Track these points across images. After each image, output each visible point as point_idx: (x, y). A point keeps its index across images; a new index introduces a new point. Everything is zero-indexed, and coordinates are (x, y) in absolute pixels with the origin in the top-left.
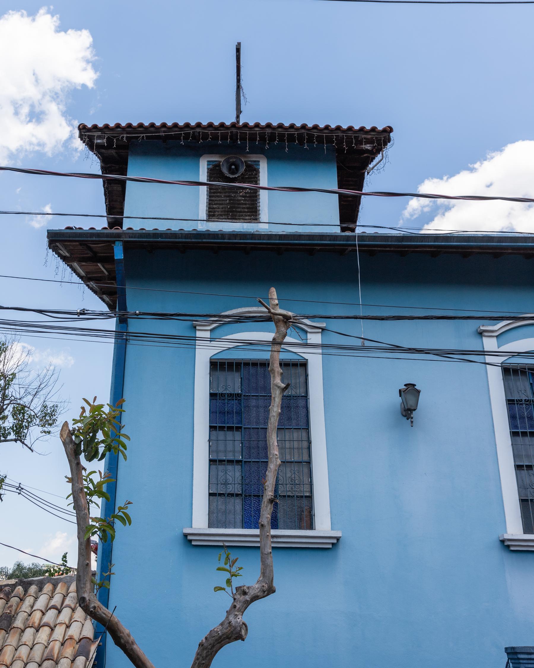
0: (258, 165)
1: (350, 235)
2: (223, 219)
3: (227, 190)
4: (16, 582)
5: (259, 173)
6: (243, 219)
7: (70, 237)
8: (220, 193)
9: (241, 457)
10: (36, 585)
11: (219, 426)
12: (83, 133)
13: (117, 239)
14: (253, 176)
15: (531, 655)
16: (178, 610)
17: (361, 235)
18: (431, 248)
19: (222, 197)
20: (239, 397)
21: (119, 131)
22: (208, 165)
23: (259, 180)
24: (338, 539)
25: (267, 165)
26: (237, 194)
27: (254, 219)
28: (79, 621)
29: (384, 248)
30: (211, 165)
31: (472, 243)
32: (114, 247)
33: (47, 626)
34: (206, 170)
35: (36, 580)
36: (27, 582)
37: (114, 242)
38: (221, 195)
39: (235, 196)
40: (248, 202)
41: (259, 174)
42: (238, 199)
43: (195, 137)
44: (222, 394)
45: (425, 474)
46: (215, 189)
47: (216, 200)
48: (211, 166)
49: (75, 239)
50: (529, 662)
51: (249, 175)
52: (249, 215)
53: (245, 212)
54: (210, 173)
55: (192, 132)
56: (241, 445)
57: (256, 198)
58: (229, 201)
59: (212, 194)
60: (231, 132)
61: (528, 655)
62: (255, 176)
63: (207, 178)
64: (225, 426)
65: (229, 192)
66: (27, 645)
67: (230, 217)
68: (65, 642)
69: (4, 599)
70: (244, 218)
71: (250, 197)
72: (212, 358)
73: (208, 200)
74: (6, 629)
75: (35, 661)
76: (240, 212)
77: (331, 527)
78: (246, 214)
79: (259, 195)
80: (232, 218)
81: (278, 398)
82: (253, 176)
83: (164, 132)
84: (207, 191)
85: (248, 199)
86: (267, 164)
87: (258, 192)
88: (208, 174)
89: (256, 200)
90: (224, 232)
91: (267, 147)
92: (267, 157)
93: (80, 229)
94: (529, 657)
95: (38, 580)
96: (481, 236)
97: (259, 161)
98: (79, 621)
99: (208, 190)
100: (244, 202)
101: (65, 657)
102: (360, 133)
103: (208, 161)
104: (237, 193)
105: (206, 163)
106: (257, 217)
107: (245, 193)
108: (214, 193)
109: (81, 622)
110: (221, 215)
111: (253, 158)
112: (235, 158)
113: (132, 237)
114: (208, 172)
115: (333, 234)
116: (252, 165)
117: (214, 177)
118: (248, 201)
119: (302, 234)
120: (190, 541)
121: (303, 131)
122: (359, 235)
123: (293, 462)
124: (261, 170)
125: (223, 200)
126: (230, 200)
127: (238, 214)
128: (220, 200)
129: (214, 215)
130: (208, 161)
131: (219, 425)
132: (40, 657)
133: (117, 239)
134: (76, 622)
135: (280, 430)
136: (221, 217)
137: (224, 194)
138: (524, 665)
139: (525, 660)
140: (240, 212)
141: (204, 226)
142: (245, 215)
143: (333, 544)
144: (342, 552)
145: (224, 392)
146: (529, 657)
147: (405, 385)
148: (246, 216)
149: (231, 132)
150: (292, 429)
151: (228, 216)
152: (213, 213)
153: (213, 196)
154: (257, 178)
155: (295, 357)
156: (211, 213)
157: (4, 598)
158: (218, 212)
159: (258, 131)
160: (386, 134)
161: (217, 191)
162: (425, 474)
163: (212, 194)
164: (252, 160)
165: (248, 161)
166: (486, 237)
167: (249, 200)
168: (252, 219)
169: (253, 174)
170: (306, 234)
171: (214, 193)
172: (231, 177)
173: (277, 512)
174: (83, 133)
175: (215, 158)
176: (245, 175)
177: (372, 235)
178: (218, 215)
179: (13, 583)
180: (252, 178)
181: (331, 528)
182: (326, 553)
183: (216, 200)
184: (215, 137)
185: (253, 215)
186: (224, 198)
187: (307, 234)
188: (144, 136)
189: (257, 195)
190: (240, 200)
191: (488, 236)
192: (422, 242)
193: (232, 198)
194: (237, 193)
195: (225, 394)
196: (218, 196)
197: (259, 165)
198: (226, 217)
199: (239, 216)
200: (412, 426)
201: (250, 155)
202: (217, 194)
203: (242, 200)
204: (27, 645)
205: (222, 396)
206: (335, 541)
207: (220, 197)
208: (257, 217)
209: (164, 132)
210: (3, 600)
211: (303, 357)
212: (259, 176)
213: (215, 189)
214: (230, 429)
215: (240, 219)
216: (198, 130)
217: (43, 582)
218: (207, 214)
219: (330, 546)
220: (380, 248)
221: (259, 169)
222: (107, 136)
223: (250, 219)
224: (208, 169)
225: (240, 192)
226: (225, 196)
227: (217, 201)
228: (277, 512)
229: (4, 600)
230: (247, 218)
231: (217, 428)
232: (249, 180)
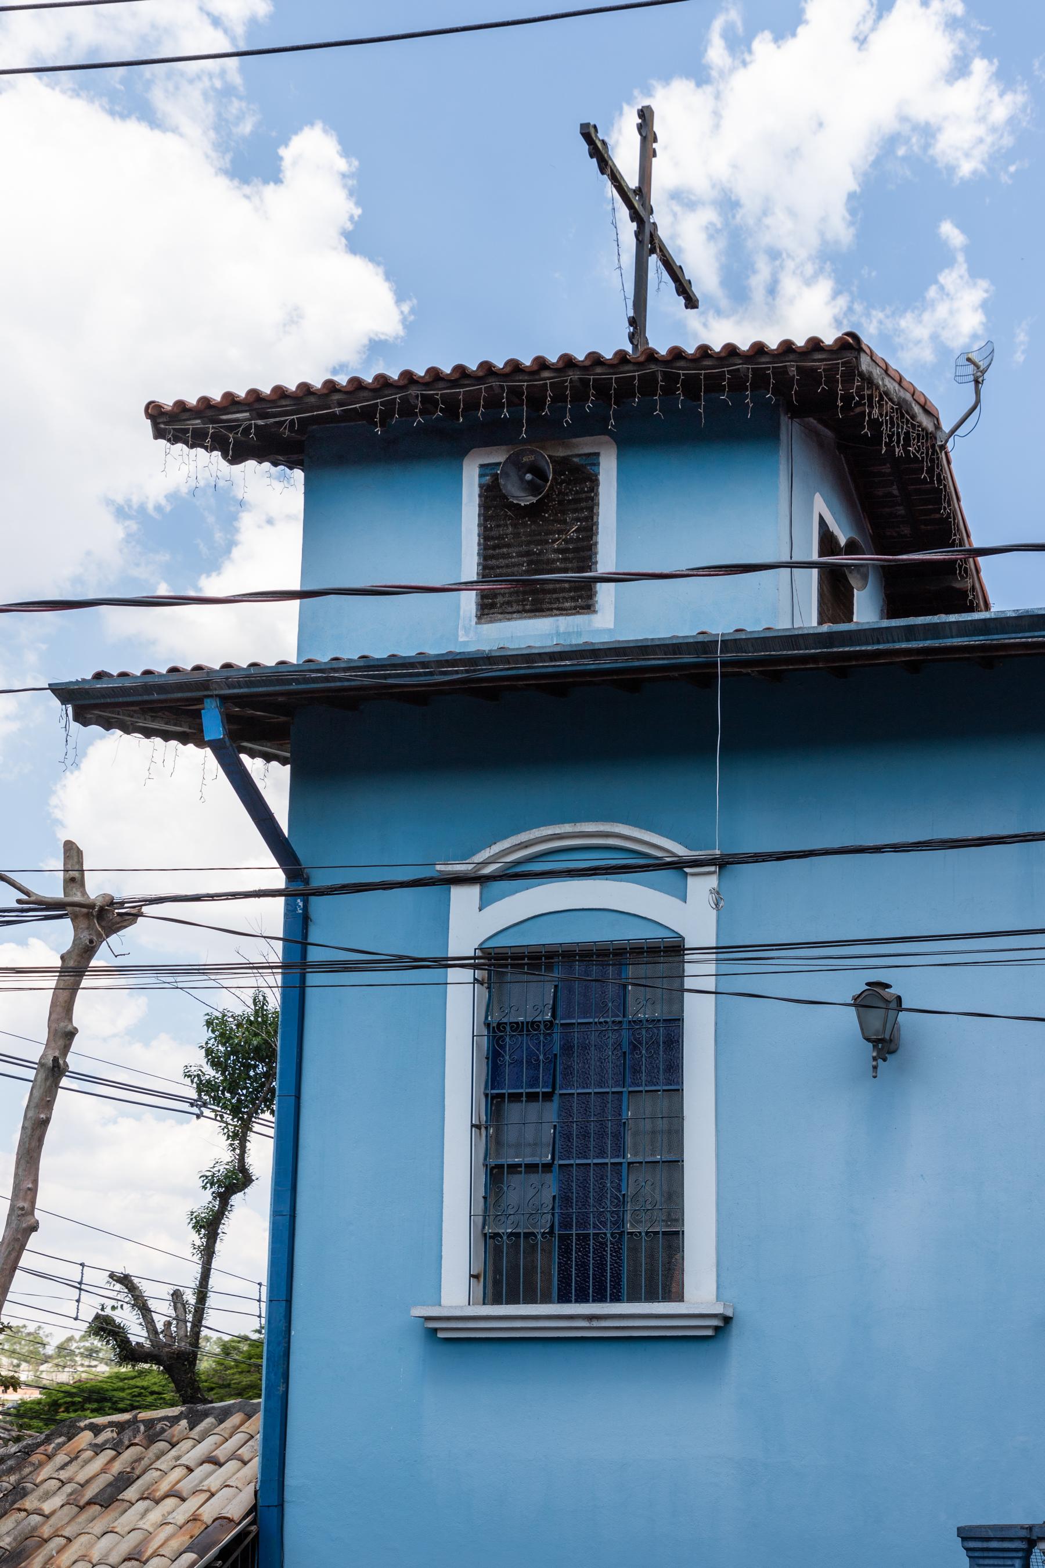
0: (594, 464)
1: (706, 640)
2: (514, 612)
3: (523, 538)
4: (182, 1413)
5: (598, 485)
6: (558, 609)
7: (103, 696)
8: (508, 546)
9: (550, 1156)
10: (215, 1418)
11: (543, 1093)
12: (162, 426)
13: (206, 693)
14: (584, 496)
15: (988, 1541)
16: (415, 1461)
17: (762, 635)
18: (911, 656)
19: (513, 557)
20: (502, 1032)
21: (286, 406)
22: (481, 476)
23: (598, 505)
24: (727, 1320)
25: (616, 460)
26: (547, 546)
27: (582, 608)
28: (232, 1487)
29: (803, 664)
30: (487, 475)
31: (998, 634)
32: (203, 711)
33: (174, 1496)
34: (476, 491)
35: (219, 1407)
36: (202, 1411)
37: (200, 700)
38: (510, 550)
39: (541, 553)
40: (570, 565)
41: (597, 489)
42: (548, 560)
43: (451, 407)
44: (533, 1023)
45: (922, 1176)
46: (498, 538)
47: (498, 567)
48: (488, 478)
49: (117, 700)
50: (986, 1554)
51: (577, 492)
52: (573, 599)
53: (563, 590)
54: (486, 497)
55: (399, 398)
56: (552, 1131)
57: (589, 553)
58: (528, 565)
59: (491, 552)
60: (490, 389)
61: (983, 1541)
62: (588, 495)
63: (479, 510)
64: (522, 1093)
65: (529, 543)
66: (116, 1533)
67: (528, 607)
68: (82, 1533)
69: (141, 1446)
70: (561, 605)
71: (576, 550)
72: (483, 947)
73: (480, 567)
74: (102, 1503)
75: (106, 1562)
76: (554, 591)
77: (715, 1293)
78: (566, 595)
79: (596, 543)
80: (534, 607)
81: (40, 1088)
82: (584, 496)
83: (340, 404)
84: (479, 544)
85: (571, 556)
86: (618, 459)
87: (594, 537)
88: (480, 500)
89: (590, 558)
90: (378, 659)
91: (567, 422)
92: (617, 445)
93: (123, 675)
94: (985, 1545)
95: (222, 1407)
96: (1014, 615)
97: (598, 454)
98: (232, 1487)
99: (482, 541)
100: (563, 566)
101: (158, 1555)
102: (787, 359)
103: (482, 466)
104: (547, 542)
105: (476, 472)
106: (590, 602)
107: (566, 541)
108: (494, 547)
109: (237, 1487)
110: (509, 603)
111: (585, 446)
112: (532, 452)
113: (235, 688)
114: (480, 496)
115: (667, 642)
116: (584, 466)
117: (495, 507)
118: (570, 560)
119: (597, 647)
120: (436, 1330)
121: (654, 367)
122: (727, 638)
123: (658, 1162)
124: (602, 478)
125: (514, 565)
126: (529, 563)
127: (549, 596)
128: (507, 566)
129: (492, 606)
130: (482, 466)
131: (510, 1091)
132: (123, 1554)
133: (206, 693)
134: (227, 1488)
135: (633, 1094)
136: (510, 609)
137: (516, 549)
138: (977, 1560)
139: (977, 1551)
140: (554, 591)
141: (472, 634)
142: (564, 598)
143: (717, 1329)
144: (738, 1342)
145: (538, 1019)
146: (985, 1545)
147: (868, 984)
148: (566, 599)
149: (490, 389)
150: (659, 1091)
151: (524, 605)
152: (490, 601)
153: (492, 557)
154: (592, 499)
155: (662, 933)
156: (486, 601)
157: (140, 1443)
158: (503, 595)
159: (549, 378)
160: (849, 355)
161: (502, 541)
162: (922, 1176)
163: (491, 552)
164: (582, 452)
165: (572, 456)
166: (1025, 616)
167: (573, 558)
168: (579, 607)
169: (584, 488)
170: (606, 647)
171: (494, 547)
172: (523, 505)
173: (621, 1266)
174: (162, 426)
175: (498, 456)
176: (567, 494)
177: (756, 636)
178: (502, 605)
179: (175, 1414)
180: (580, 500)
181: (717, 1299)
182: (703, 1346)
183: (498, 567)
184: (494, 403)
185: (581, 597)
186: (516, 560)
187: (608, 647)
188: (294, 419)
189: (592, 545)
190: (554, 561)
191: (1030, 613)
192: (879, 643)
193: (534, 557)
194: (547, 542)
195: (540, 1022)
196: (505, 556)
197: (598, 464)
198: (520, 608)
199: (551, 603)
200: (875, 1077)
201: (578, 439)
202: (501, 551)
203: (558, 560)
204: (116, 1533)
205: (532, 1027)
206: (715, 1322)
207: (507, 556)
208: (590, 602)
209: (340, 404)
210: (137, 1447)
211: (676, 933)
212: (597, 494)
213: (498, 538)
214: (532, 1097)
215: (551, 609)
216: (413, 391)
217: (230, 1411)
218: (477, 604)
219: (710, 1333)
220: (792, 665)
221: (597, 475)
222: (213, 428)
223: (575, 608)
224: (481, 486)
225: (554, 541)
226: (520, 555)
227: (502, 567)
228: (621, 1266)
229: (140, 1447)
230: (567, 605)
231: (539, 1097)
232: (575, 506)
